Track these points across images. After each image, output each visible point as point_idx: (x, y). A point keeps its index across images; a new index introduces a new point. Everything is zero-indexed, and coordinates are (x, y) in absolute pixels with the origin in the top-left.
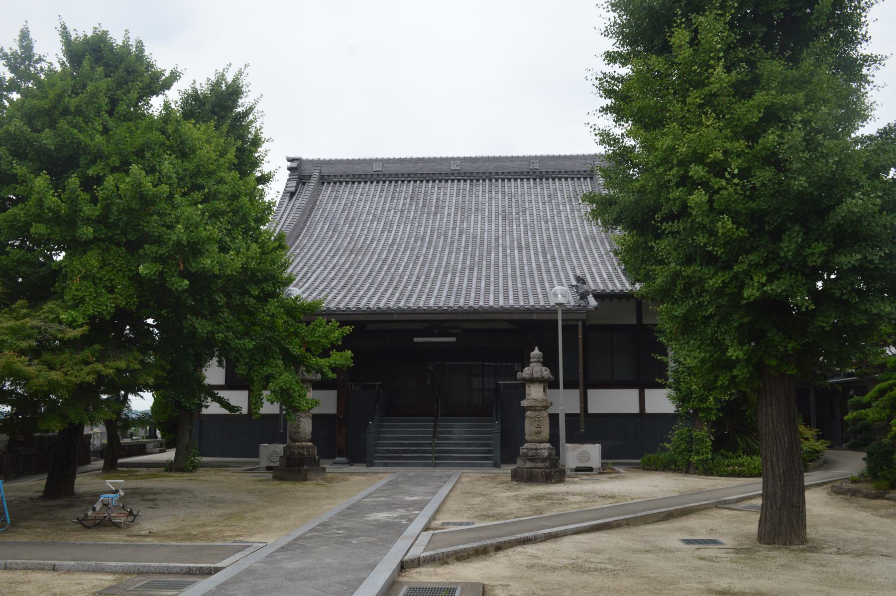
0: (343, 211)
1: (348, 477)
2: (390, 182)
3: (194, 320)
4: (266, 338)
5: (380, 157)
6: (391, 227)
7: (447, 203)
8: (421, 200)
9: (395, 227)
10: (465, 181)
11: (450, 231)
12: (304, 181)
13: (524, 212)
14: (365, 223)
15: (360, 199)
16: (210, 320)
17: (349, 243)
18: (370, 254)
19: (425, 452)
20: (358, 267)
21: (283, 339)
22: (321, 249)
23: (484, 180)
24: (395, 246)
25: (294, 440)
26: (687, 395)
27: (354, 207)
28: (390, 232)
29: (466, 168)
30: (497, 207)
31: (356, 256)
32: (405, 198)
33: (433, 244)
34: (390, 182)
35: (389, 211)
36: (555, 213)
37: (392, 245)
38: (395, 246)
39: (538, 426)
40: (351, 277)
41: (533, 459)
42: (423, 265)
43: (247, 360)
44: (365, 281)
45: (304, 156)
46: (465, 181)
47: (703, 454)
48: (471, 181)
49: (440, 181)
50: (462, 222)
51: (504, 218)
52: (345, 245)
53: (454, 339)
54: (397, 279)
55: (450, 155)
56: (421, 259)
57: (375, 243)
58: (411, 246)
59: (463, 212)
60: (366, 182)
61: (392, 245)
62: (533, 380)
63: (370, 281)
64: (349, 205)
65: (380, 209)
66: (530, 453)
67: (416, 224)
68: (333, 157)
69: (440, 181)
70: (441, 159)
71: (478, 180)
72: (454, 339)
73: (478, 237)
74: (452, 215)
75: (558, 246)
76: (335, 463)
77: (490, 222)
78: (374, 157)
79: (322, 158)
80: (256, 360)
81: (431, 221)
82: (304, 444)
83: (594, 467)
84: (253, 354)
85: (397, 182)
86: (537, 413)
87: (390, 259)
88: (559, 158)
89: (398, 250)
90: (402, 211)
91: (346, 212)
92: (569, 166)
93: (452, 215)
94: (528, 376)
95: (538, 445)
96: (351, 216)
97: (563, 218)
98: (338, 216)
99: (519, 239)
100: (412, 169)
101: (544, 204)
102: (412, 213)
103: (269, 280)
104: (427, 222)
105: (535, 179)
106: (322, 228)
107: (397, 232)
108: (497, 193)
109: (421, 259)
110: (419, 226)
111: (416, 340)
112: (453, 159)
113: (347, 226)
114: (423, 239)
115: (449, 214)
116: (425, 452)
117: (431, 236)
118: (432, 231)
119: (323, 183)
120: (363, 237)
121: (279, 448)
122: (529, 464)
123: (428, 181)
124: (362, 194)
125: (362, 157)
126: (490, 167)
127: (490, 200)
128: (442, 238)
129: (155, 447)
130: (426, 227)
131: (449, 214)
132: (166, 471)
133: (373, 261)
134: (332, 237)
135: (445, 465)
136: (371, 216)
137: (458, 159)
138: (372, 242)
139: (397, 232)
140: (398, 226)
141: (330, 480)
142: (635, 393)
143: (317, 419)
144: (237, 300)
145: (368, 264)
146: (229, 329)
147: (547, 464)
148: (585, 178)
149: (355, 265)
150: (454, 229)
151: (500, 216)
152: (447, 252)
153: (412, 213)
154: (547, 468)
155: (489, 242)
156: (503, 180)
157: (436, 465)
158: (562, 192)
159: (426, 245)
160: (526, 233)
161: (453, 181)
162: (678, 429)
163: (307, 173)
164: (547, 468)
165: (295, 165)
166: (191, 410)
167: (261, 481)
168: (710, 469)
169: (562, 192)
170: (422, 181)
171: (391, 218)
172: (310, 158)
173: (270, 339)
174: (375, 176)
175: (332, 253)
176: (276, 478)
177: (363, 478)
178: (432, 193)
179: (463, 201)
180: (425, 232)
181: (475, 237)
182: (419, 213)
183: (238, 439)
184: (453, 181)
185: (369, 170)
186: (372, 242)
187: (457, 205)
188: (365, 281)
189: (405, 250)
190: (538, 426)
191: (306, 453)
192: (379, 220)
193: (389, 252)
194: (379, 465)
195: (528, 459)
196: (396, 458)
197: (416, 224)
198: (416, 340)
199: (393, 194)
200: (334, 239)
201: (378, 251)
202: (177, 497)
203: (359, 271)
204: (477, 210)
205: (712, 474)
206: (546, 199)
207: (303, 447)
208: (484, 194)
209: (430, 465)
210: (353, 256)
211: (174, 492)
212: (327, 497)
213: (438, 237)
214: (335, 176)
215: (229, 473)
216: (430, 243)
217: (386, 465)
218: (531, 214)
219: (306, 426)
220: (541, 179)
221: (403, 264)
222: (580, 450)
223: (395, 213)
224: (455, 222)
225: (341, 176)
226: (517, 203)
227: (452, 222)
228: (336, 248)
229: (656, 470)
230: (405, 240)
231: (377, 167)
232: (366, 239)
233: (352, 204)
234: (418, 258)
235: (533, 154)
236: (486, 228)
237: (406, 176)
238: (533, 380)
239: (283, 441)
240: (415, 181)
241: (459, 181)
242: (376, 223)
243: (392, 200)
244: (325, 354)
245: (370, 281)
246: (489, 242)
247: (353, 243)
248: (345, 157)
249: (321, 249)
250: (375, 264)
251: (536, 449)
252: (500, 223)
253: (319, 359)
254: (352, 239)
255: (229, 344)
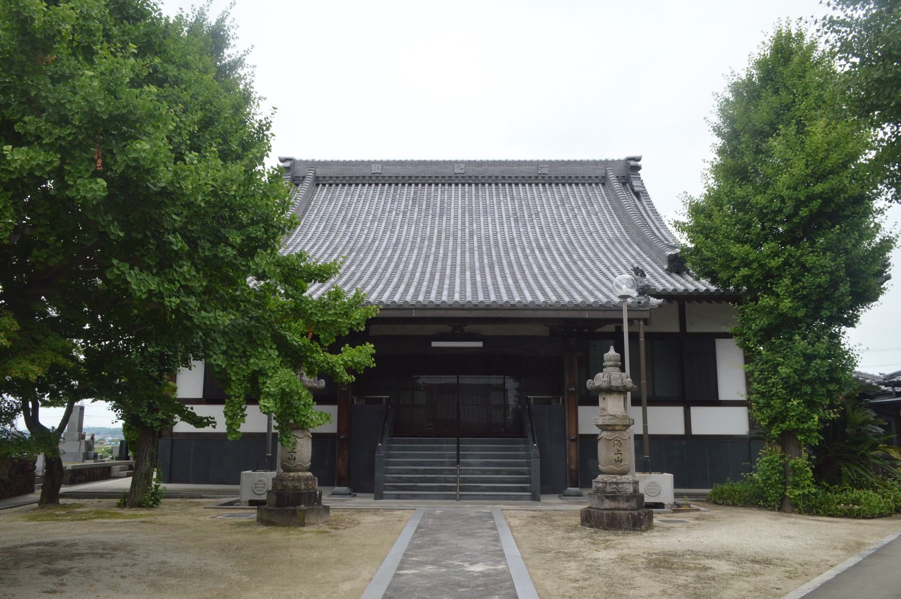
0: (340, 212)
1: (356, 517)
2: (390, 185)
3: (125, 267)
4: (251, 318)
5: (379, 159)
6: (394, 227)
7: (453, 205)
8: (425, 203)
9: (398, 227)
10: (470, 185)
11: (459, 232)
12: (297, 182)
13: (537, 214)
14: (364, 223)
15: (358, 201)
16: (157, 274)
17: (348, 242)
18: (372, 252)
19: (446, 481)
20: (360, 264)
21: (277, 321)
22: (316, 247)
23: (490, 184)
24: (400, 246)
25: (287, 469)
26: (781, 413)
27: (352, 208)
28: (392, 232)
29: (471, 171)
30: (507, 210)
31: (358, 254)
32: (407, 201)
33: (442, 244)
34: (390, 185)
35: (390, 212)
36: (571, 216)
37: (396, 245)
38: (400, 246)
39: (619, 452)
40: (353, 274)
41: (613, 497)
42: (435, 263)
43: (224, 348)
44: (371, 277)
45: (298, 157)
46: (470, 185)
47: (804, 488)
48: (477, 184)
49: (443, 184)
50: (471, 223)
51: (516, 220)
52: (344, 243)
53: (479, 344)
54: (408, 275)
55: (453, 158)
56: (432, 257)
57: (377, 242)
58: (417, 245)
59: (471, 215)
60: (364, 185)
61: (396, 245)
62: (610, 390)
63: (377, 277)
64: (346, 205)
65: (380, 210)
66: (609, 489)
67: (421, 225)
68: (329, 159)
69: (443, 184)
70: (444, 162)
71: (483, 184)
72: (479, 344)
73: (491, 238)
74: (460, 216)
75: (582, 247)
76: (334, 494)
77: (502, 224)
78: (372, 159)
79: (317, 159)
80: (236, 350)
81: (437, 222)
82: (301, 474)
83: (665, 502)
84: (232, 341)
85: (397, 184)
86: (617, 434)
87: (396, 257)
88: (569, 163)
89: (403, 250)
90: (405, 213)
91: (344, 213)
92: (579, 171)
93: (460, 216)
94: (605, 385)
95: (619, 477)
96: (349, 216)
97: (581, 222)
98: (335, 216)
99: (537, 241)
100: (413, 172)
101: (557, 207)
102: (416, 215)
103: (258, 223)
104: (433, 223)
105: (543, 184)
106: (317, 228)
107: (400, 232)
108: (505, 196)
109: (432, 257)
110: (425, 227)
111: (435, 344)
112: (456, 162)
113: (345, 226)
114: (430, 239)
115: (456, 217)
116: (446, 481)
117: (439, 237)
118: (440, 232)
119: (318, 185)
120: (364, 237)
121: (267, 477)
122: (608, 504)
123: (430, 185)
124: (360, 196)
125: (360, 158)
126: (496, 171)
127: (499, 203)
128: (451, 238)
129: (122, 470)
130: (432, 228)
131: (456, 217)
132: (119, 506)
133: (377, 258)
134: (328, 236)
135: (472, 497)
136: (371, 217)
137: (462, 162)
138: (373, 241)
139: (400, 232)
140: (402, 227)
141: (336, 525)
142: (679, 411)
143: (317, 439)
144: (205, 249)
145: (371, 262)
146: (189, 291)
147: (633, 504)
148: (597, 184)
149: (357, 262)
150: (463, 230)
151: (512, 219)
152: (459, 252)
153: (416, 215)
154: (633, 509)
155: (505, 244)
156: (510, 184)
157: (462, 497)
158: (574, 197)
159: (434, 245)
160: (543, 235)
161: (457, 184)
162: (765, 455)
163: (300, 174)
164: (633, 509)
165: (287, 164)
166: (152, 427)
167: (241, 525)
168: (815, 506)
169: (574, 197)
170: (423, 185)
171: (393, 218)
172: (304, 159)
173: (258, 319)
174: (374, 178)
175: (329, 251)
176: (263, 521)
177: (378, 519)
178: (436, 196)
179: (470, 204)
180: (432, 233)
181: (488, 238)
182: (423, 214)
183: (215, 462)
184: (457, 184)
185: (367, 172)
186: (373, 241)
187: (463, 208)
188: (371, 277)
189: (412, 250)
190: (619, 452)
191: (303, 487)
192: (380, 221)
193: (394, 251)
194: (390, 497)
195: (607, 497)
196: (410, 488)
197: (421, 225)
198: (435, 344)
199: (394, 196)
200: (331, 238)
201: (382, 249)
202: (105, 563)
203: (363, 268)
204: (486, 212)
205: (818, 514)
206: (559, 203)
207: (299, 479)
208: (491, 197)
209: (454, 497)
210: (354, 254)
211: (107, 551)
212: (340, 561)
213: (447, 238)
214: (331, 177)
215: (200, 509)
216: (439, 243)
217: (398, 497)
218: (545, 217)
219: (304, 449)
220: (550, 184)
221: (412, 262)
222: (648, 481)
223: (397, 214)
224: (463, 223)
225: (337, 177)
226: (528, 206)
227: (460, 223)
228: (333, 247)
229: (734, 505)
230: (411, 239)
231: (375, 169)
232: (366, 239)
233: (350, 205)
234: (427, 257)
235: (541, 158)
236: (498, 230)
237: (407, 178)
238: (610, 390)
239: (272, 468)
240: (417, 185)
241: (463, 184)
242: (376, 223)
243: (393, 202)
244: (335, 349)
245: (377, 277)
246: (505, 244)
247: (353, 242)
248: (341, 159)
249: (316, 247)
250: (380, 262)
251: (617, 483)
252: (513, 225)
253: (328, 355)
254: (351, 238)
255: (190, 319)
